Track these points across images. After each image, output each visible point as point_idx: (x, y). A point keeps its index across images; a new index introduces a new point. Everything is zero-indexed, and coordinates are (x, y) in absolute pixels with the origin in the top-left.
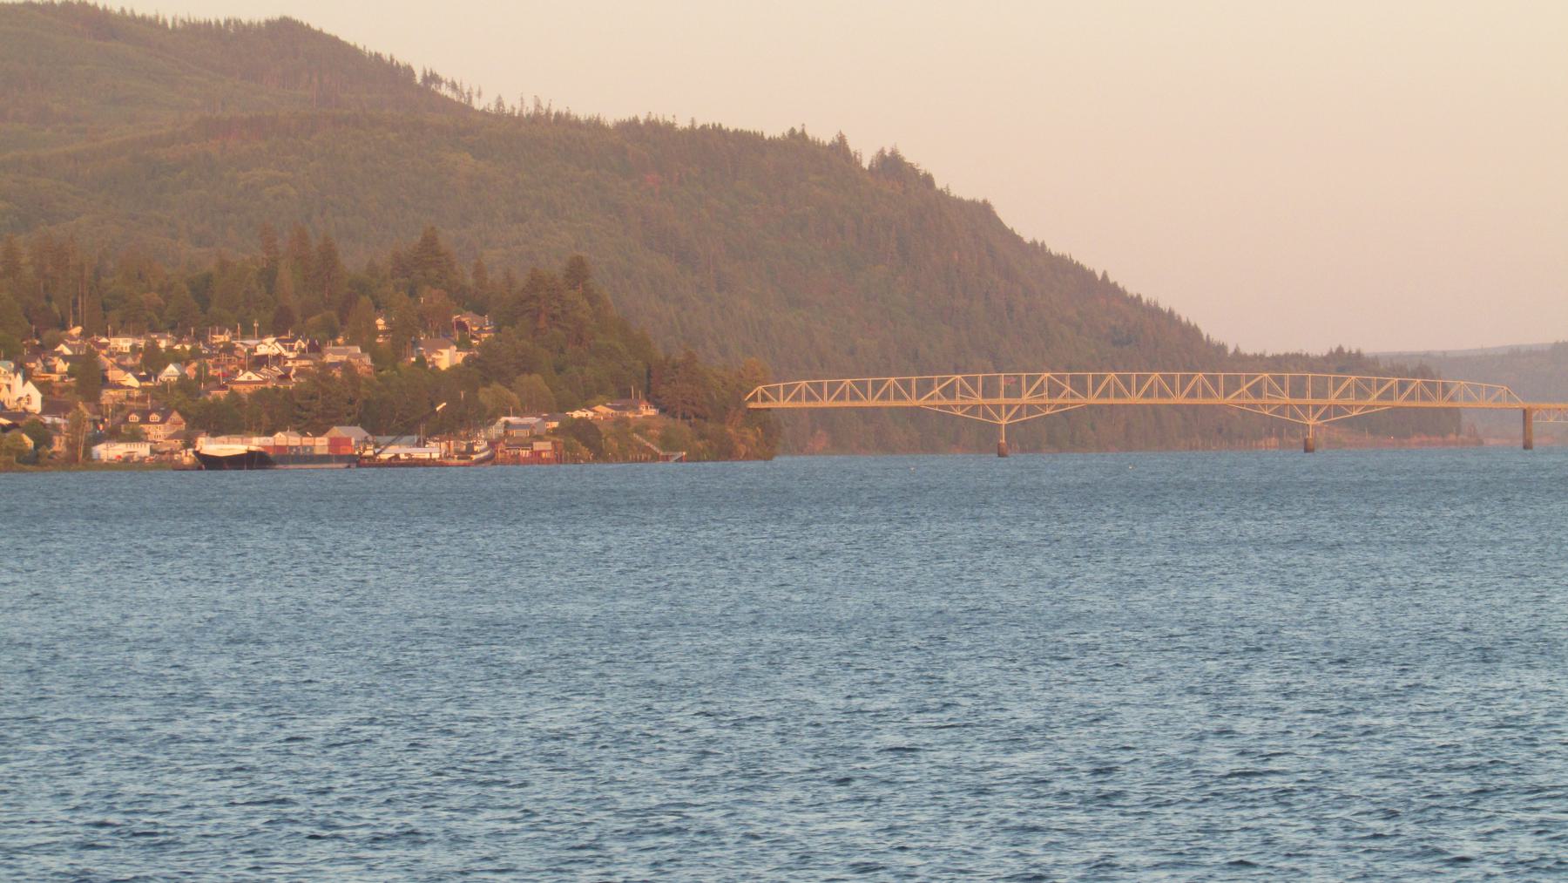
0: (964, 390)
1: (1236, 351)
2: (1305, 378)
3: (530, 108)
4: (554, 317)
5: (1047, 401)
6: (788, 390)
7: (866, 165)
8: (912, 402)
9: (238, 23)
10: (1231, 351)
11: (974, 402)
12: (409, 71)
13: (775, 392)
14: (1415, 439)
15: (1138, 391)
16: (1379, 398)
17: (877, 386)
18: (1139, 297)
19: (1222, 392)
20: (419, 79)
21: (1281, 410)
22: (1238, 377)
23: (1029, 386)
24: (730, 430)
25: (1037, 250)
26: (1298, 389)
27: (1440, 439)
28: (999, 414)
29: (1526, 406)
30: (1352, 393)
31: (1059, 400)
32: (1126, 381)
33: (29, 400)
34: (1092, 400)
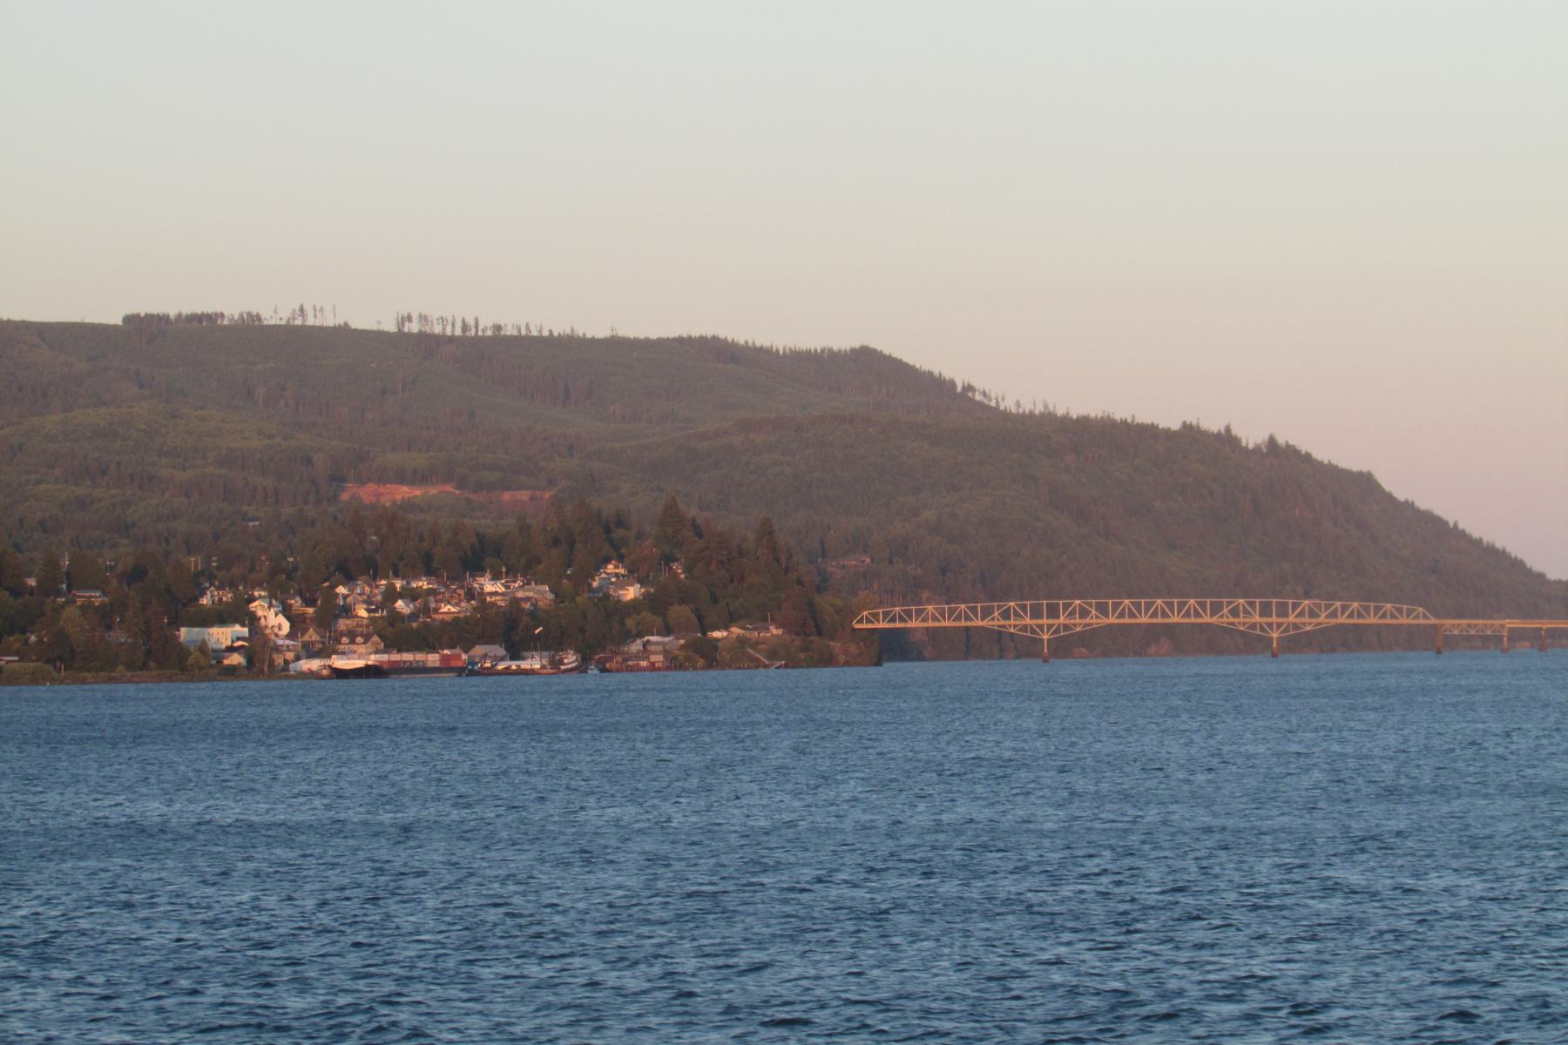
0: (1246, 611)
3: (1039, 409)
4: (722, 562)
8: (1207, 619)
9: (830, 350)
12: (952, 383)
13: (875, 616)
20: (959, 389)
21: (1253, 626)
23: (1114, 611)
25: (1409, 506)
31: (1088, 621)
32: (1138, 606)
33: (280, 628)
34: (1112, 620)
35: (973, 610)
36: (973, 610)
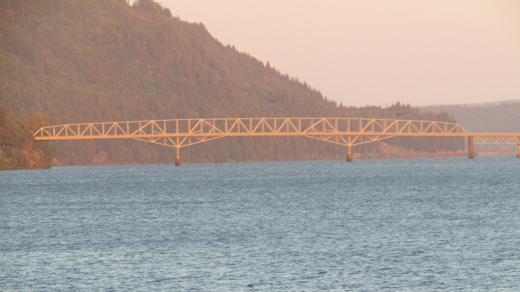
0: (156, 129)
1: (341, 105)
2: (175, 121)
5: (202, 134)
6: (58, 130)
7: (131, 4)
8: (127, 136)
10: (338, 105)
11: (333, 134)
14: (439, 153)
15: (278, 128)
16: (388, 131)
17: (107, 127)
18: (287, 75)
19: (300, 128)
21: (162, 140)
22: (138, 124)
24: (25, 152)
25: (230, 50)
26: (342, 127)
27: (453, 153)
28: (176, 142)
29: (470, 134)
30: (410, 129)
31: (209, 134)
35: (442, 126)
36: (124, 126)
